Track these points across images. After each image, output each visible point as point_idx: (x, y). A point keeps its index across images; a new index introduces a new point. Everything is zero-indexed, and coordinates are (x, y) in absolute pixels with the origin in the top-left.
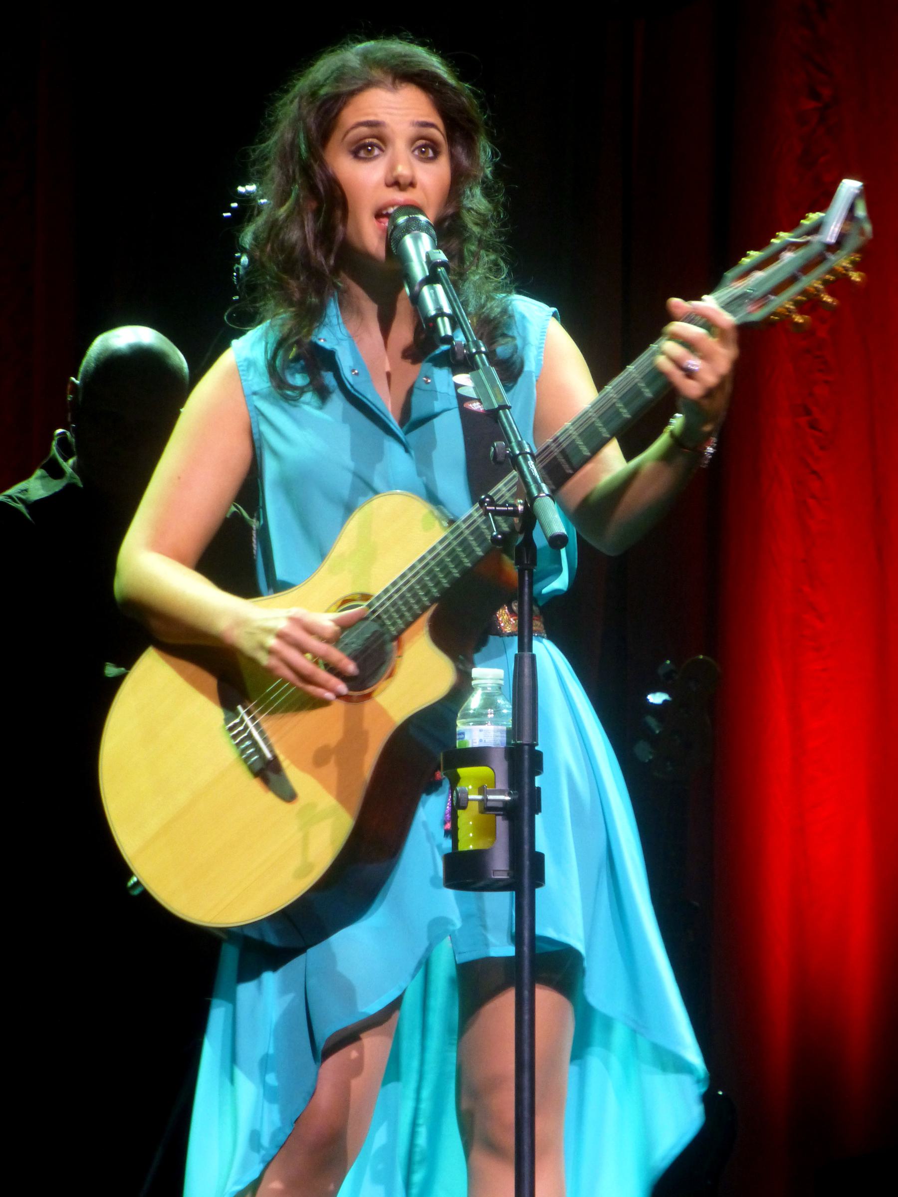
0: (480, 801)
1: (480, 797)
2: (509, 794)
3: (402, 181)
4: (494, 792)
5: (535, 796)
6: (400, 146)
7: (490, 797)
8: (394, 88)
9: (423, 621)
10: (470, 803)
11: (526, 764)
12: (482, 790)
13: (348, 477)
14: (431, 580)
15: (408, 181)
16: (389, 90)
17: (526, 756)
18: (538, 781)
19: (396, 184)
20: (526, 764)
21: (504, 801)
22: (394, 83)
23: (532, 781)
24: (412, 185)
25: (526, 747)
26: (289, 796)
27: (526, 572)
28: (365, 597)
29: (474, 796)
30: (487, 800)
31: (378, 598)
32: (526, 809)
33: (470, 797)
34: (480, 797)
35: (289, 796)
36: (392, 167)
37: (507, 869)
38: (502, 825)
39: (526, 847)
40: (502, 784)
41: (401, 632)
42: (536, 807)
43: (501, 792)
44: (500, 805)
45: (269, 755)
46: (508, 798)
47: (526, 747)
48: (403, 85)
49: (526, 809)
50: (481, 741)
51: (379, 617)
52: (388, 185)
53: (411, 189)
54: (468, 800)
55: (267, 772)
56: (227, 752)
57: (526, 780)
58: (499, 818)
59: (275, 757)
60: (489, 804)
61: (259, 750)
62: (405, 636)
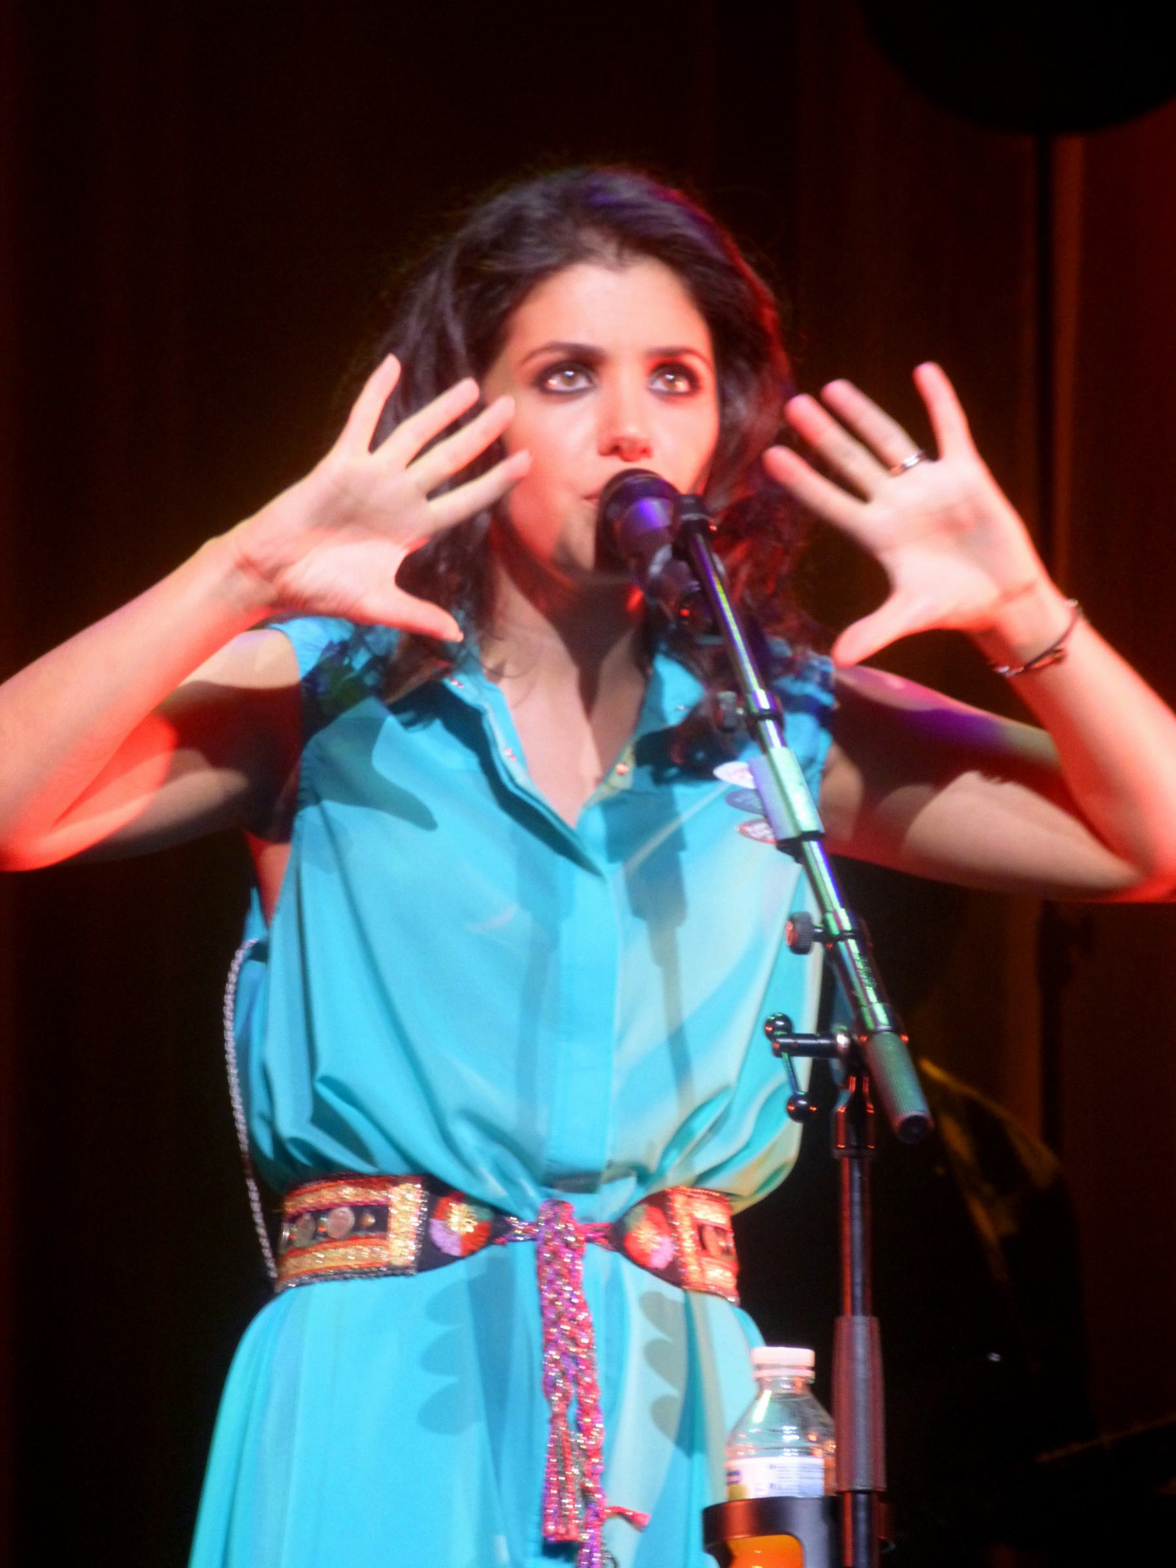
3: (625, 446)
6: (628, 379)
8: (619, 265)
16: (610, 267)
19: (615, 449)
22: (619, 255)
36: (610, 420)
48: (638, 258)
50: (772, 1486)
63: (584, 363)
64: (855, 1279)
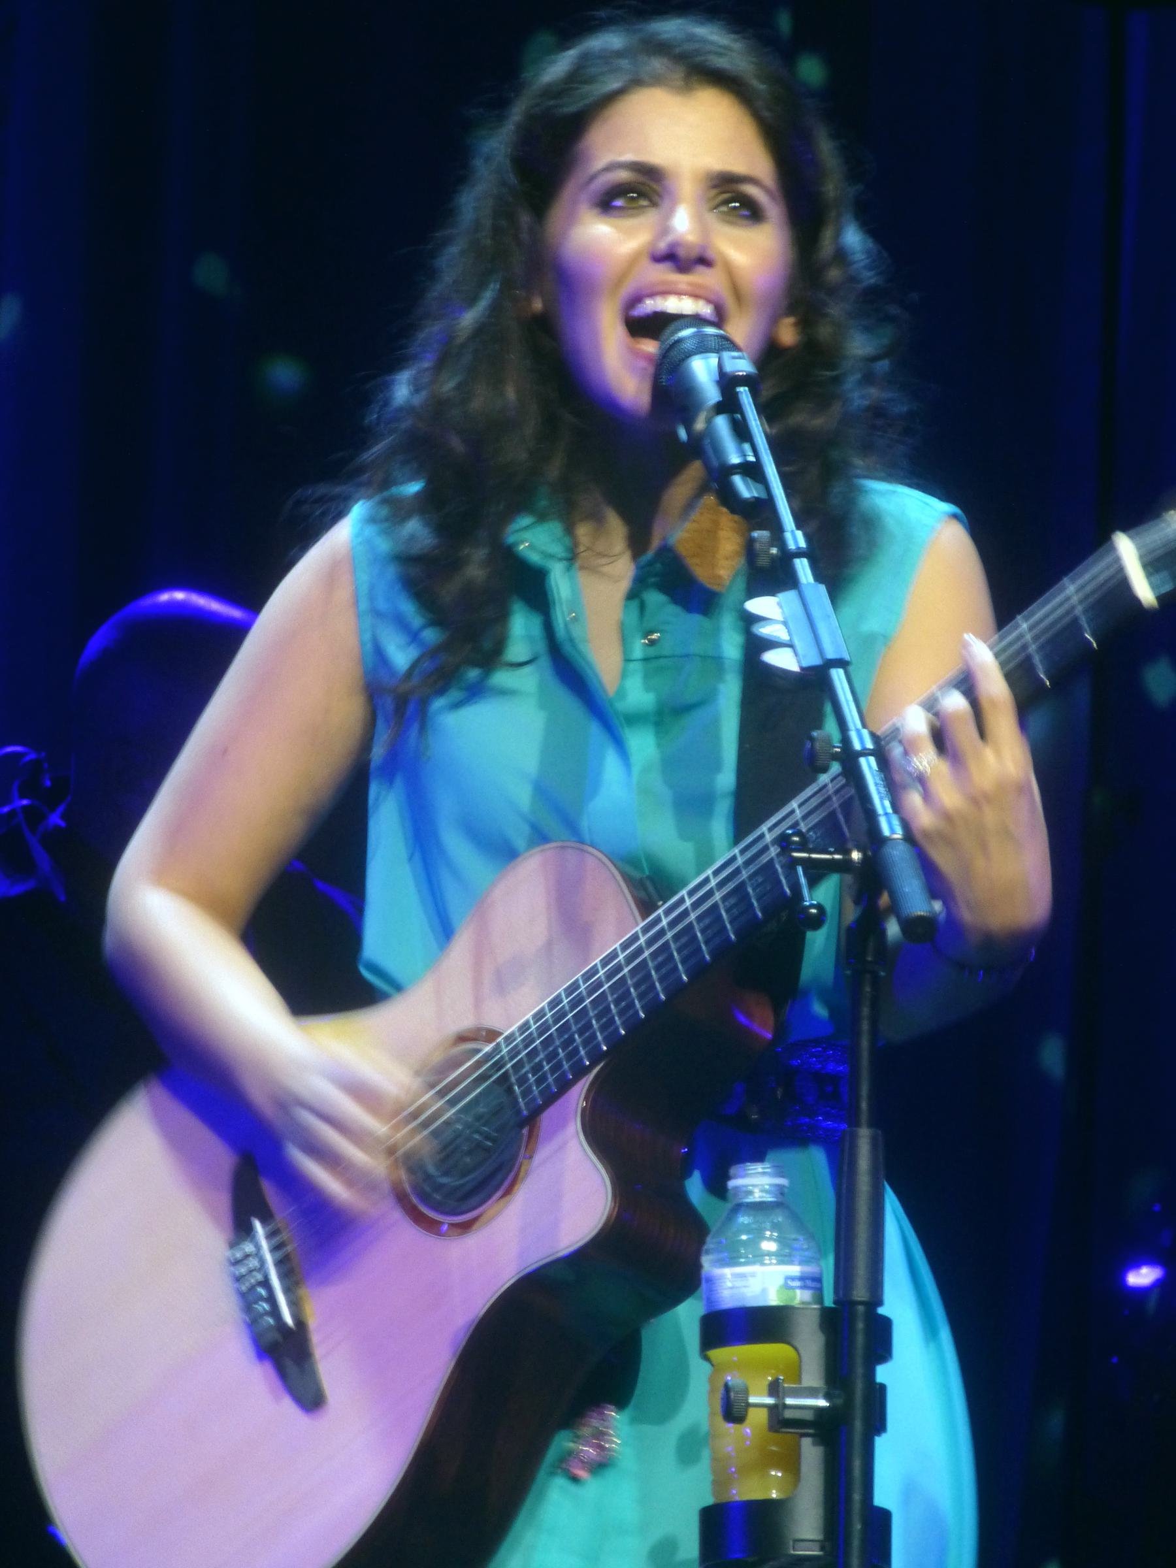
0: (771, 1408)
1: (770, 1401)
2: (827, 1397)
3: (682, 253)
4: (796, 1393)
5: (877, 1397)
7: (789, 1401)
9: (578, 1096)
10: (752, 1412)
11: (860, 1339)
12: (774, 1389)
13: (523, 796)
14: (599, 1017)
15: (694, 254)
17: (860, 1325)
18: (882, 1373)
20: (860, 1339)
21: (819, 1410)
23: (870, 1374)
24: (704, 261)
25: (861, 1308)
26: (311, 1400)
27: (868, 976)
28: (492, 1035)
29: (760, 1398)
30: (786, 1406)
31: (510, 1039)
32: (858, 1425)
33: (752, 1400)
34: (770, 1401)
35: (311, 1400)
37: (820, 1537)
38: (811, 1454)
39: (857, 1497)
40: (813, 1376)
41: (536, 1112)
42: (876, 1422)
43: (812, 1392)
44: (808, 1416)
45: (288, 1319)
46: (822, 1403)
47: (861, 1308)
49: (858, 1425)
51: (505, 1076)
52: (658, 259)
53: (701, 269)
54: (748, 1405)
55: (285, 1353)
56: (224, 1309)
57: (860, 1370)
58: (806, 1442)
59: (300, 1323)
60: (788, 1414)
61: (275, 1311)
62: (546, 1117)
63: (643, 188)
64: (864, 1116)
